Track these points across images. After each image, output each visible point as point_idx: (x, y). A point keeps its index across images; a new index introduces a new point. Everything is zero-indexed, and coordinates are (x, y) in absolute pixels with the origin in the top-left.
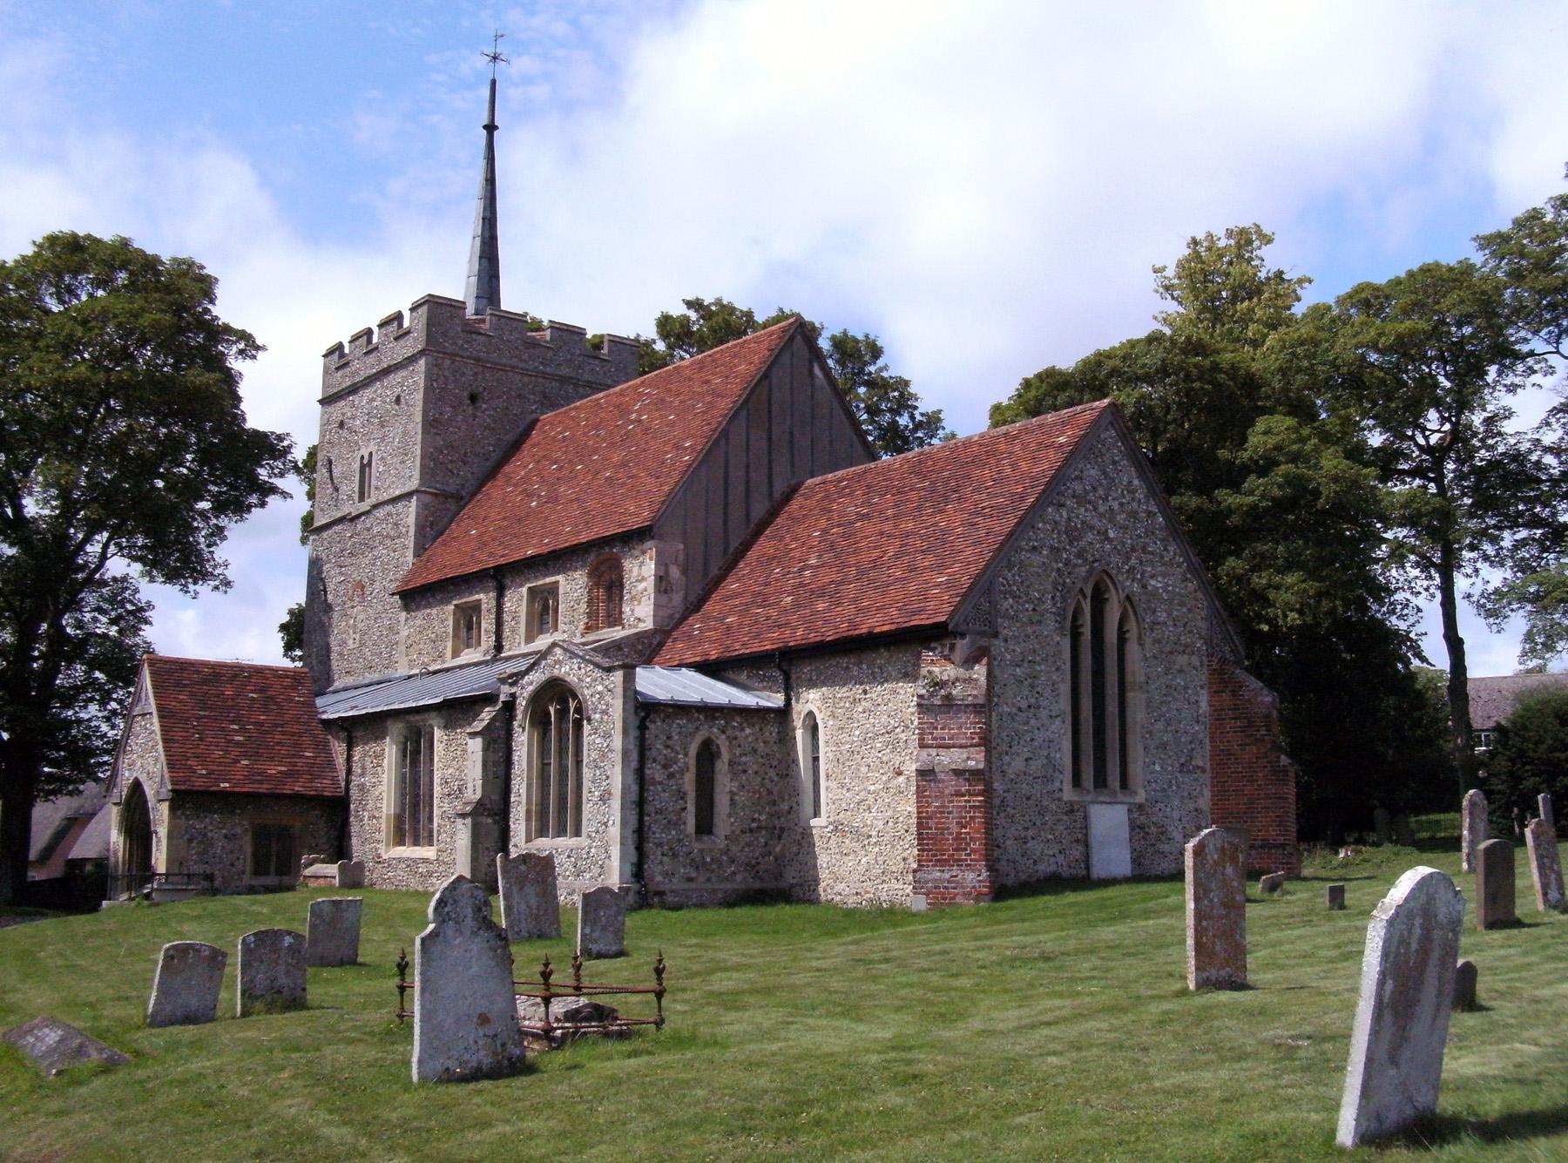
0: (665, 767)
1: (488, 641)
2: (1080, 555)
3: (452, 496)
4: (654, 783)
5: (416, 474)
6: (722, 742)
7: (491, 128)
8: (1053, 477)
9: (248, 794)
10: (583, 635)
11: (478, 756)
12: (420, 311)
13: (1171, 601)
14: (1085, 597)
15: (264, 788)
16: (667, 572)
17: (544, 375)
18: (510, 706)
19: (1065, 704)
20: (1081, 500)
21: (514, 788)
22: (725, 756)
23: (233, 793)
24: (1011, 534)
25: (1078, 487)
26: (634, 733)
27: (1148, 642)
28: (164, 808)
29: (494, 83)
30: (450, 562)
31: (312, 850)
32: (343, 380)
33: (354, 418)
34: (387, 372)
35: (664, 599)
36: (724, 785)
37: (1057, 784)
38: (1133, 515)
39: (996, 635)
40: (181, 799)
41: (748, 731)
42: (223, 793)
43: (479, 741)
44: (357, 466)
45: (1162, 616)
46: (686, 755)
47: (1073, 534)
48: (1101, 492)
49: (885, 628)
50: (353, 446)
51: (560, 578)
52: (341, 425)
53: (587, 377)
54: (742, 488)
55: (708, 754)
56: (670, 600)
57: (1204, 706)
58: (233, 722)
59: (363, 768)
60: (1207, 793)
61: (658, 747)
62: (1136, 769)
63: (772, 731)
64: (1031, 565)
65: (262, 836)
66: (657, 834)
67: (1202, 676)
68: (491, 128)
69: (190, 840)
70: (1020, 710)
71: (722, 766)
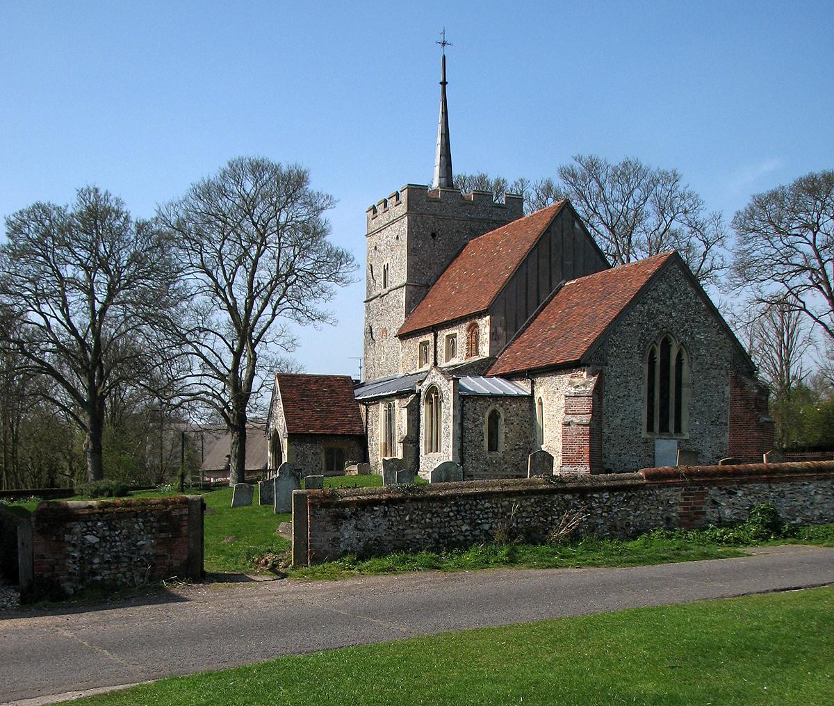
0: (473, 422)
1: (431, 361)
2: (655, 325)
3: (424, 286)
4: (469, 429)
5: (406, 277)
6: (501, 411)
7: (444, 83)
8: (639, 291)
9: (321, 435)
10: (446, 362)
11: (405, 418)
12: (404, 191)
13: (709, 344)
14: (657, 345)
15: (329, 432)
16: (496, 331)
17: (471, 219)
18: (419, 395)
19: (644, 394)
20: (656, 300)
21: (421, 431)
22: (503, 417)
23: (315, 434)
24: (615, 318)
25: (654, 294)
26: (458, 408)
27: (694, 364)
28: (286, 441)
29: (444, 57)
30: (421, 321)
31: (352, 459)
32: (374, 225)
33: (380, 245)
34: (392, 222)
35: (495, 343)
36: (503, 429)
37: (639, 430)
38: (688, 305)
39: (606, 364)
40: (292, 437)
41: (514, 406)
42: (311, 435)
43: (406, 409)
44: (382, 270)
45: (703, 352)
46: (483, 417)
47: (651, 316)
48: (668, 295)
49: (561, 361)
50: (381, 260)
51: (457, 331)
52: (376, 248)
53: (494, 218)
54: (535, 288)
55: (494, 418)
56: (498, 343)
57: (728, 394)
58: (316, 402)
59: (372, 422)
60: (727, 435)
61: (470, 415)
62: (684, 424)
63: (526, 405)
64: (626, 332)
65: (329, 452)
66: (470, 451)
67: (728, 380)
68: (444, 83)
69: (297, 455)
70: (619, 397)
71: (501, 422)
